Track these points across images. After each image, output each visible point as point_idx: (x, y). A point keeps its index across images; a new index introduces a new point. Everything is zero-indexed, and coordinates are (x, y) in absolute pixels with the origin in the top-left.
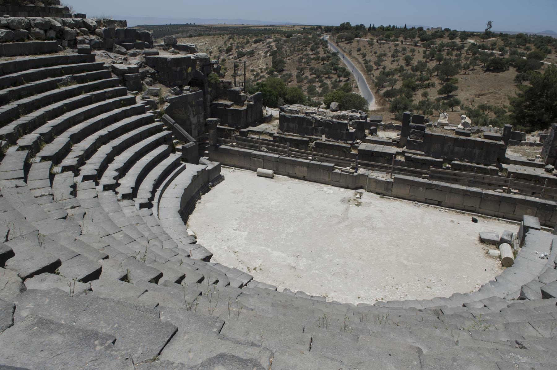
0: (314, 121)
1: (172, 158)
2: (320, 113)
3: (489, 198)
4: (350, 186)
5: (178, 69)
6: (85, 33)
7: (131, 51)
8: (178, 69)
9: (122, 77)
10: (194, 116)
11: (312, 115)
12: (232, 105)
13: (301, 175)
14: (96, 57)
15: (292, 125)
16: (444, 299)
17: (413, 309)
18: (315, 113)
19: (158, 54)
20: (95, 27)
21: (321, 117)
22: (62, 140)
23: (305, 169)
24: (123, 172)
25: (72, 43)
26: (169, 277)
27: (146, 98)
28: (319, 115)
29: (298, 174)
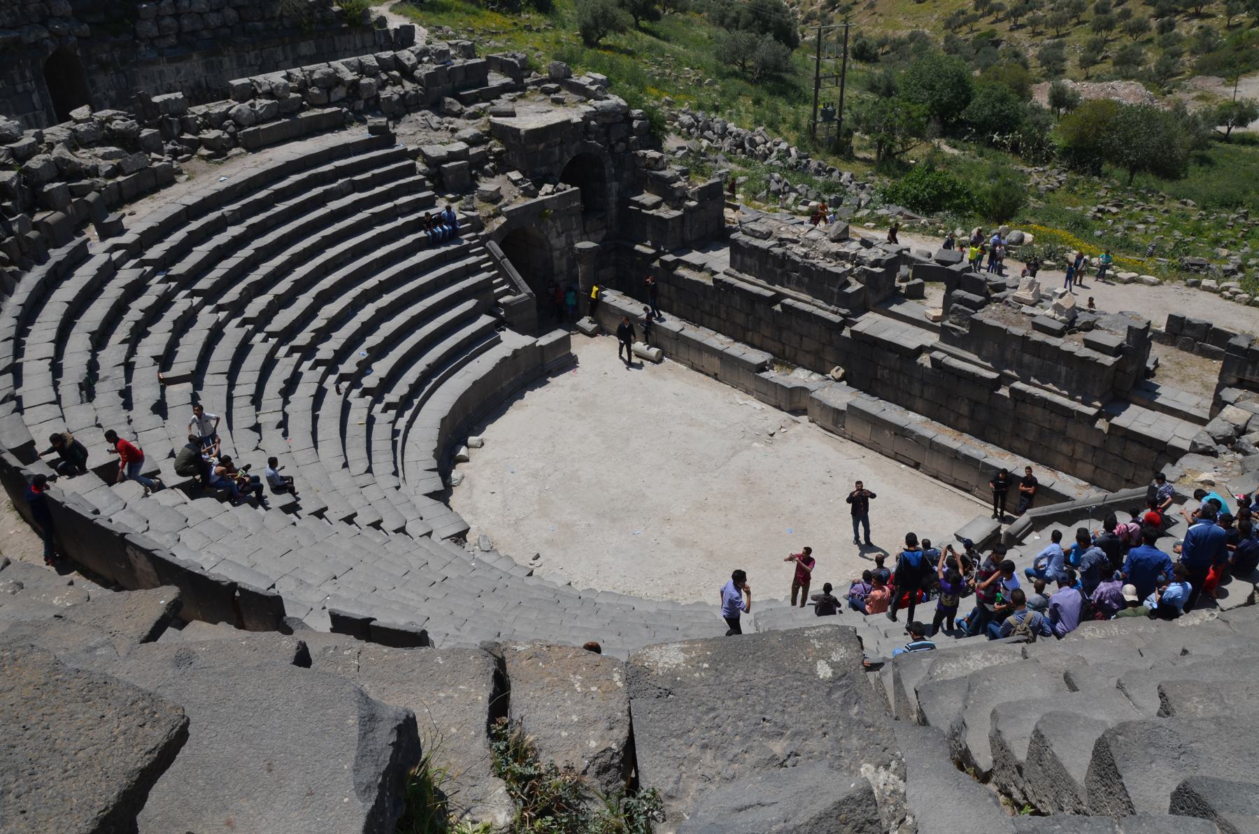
1: (485, 320)
4: (782, 404)
5: (542, 146)
6: (397, 82)
7: (471, 109)
9: (435, 170)
10: (559, 235)
12: (656, 206)
13: (712, 371)
14: (398, 139)
15: (748, 261)
18: (795, 242)
19: (512, 114)
20: (414, 67)
22: (304, 300)
23: (716, 361)
24: (379, 352)
25: (372, 102)
26: (363, 519)
28: (803, 246)
29: (707, 368)
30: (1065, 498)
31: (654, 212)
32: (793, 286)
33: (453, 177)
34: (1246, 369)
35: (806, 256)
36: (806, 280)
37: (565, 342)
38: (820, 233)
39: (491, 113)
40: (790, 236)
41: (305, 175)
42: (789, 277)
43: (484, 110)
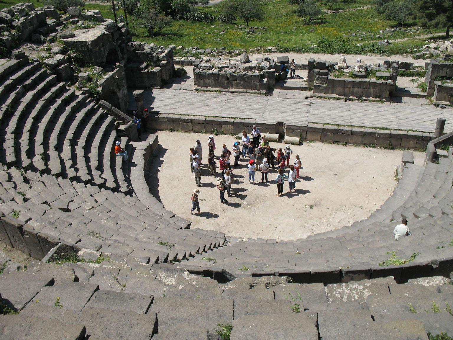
0: (230, 87)
2: (233, 66)
3: (382, 136)
5: (97, 48)
8: (97, 48)
11: (225, 69)
16: (348, 227)
17: (329, 239)
18: (227, 67)
19: (73, 36)
21: (233, 70)
27: (82, 88)
28: (232, 68)
30: (447, 133)
31: (146, 71)
32: (235, 87)
33: (65, 74)
34: (439, 72)
35: (235, 72)
36: (242, 82)
37: (157, 140)
38: (235, 60)
39: (60, 37)
40: (224, 65)
41: (44, 83)
42: (232, 83)
43: (55, 36)
